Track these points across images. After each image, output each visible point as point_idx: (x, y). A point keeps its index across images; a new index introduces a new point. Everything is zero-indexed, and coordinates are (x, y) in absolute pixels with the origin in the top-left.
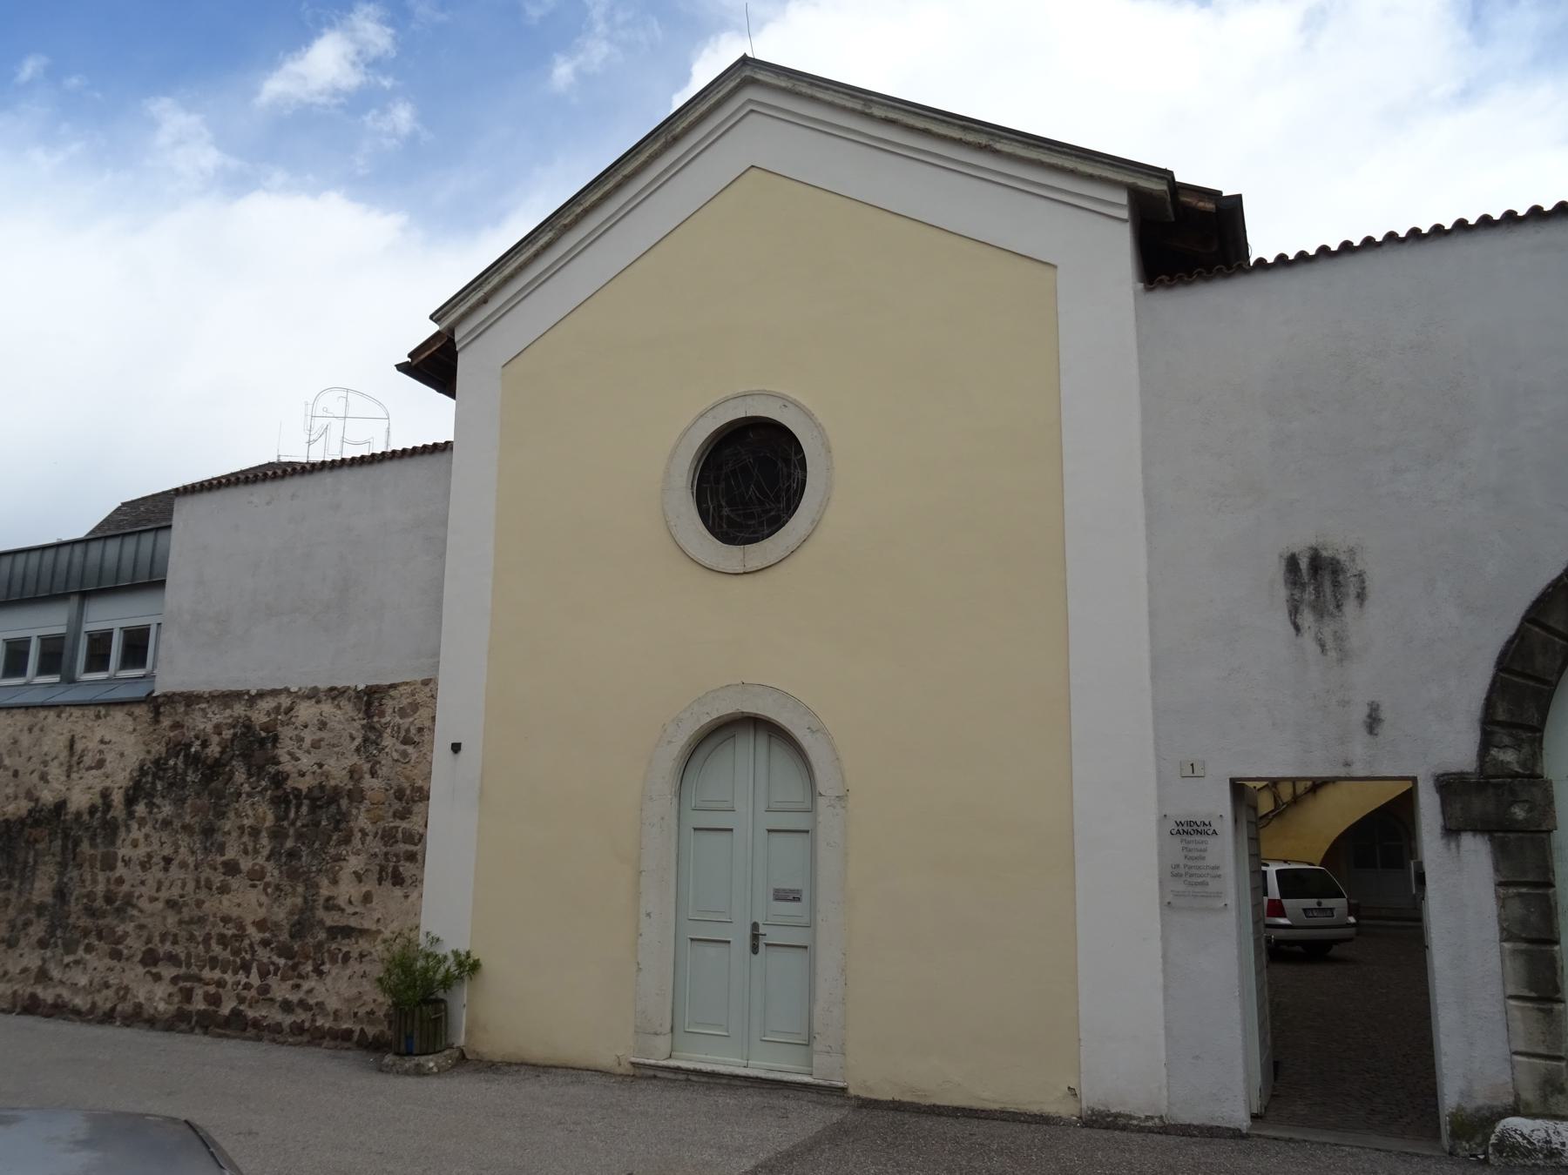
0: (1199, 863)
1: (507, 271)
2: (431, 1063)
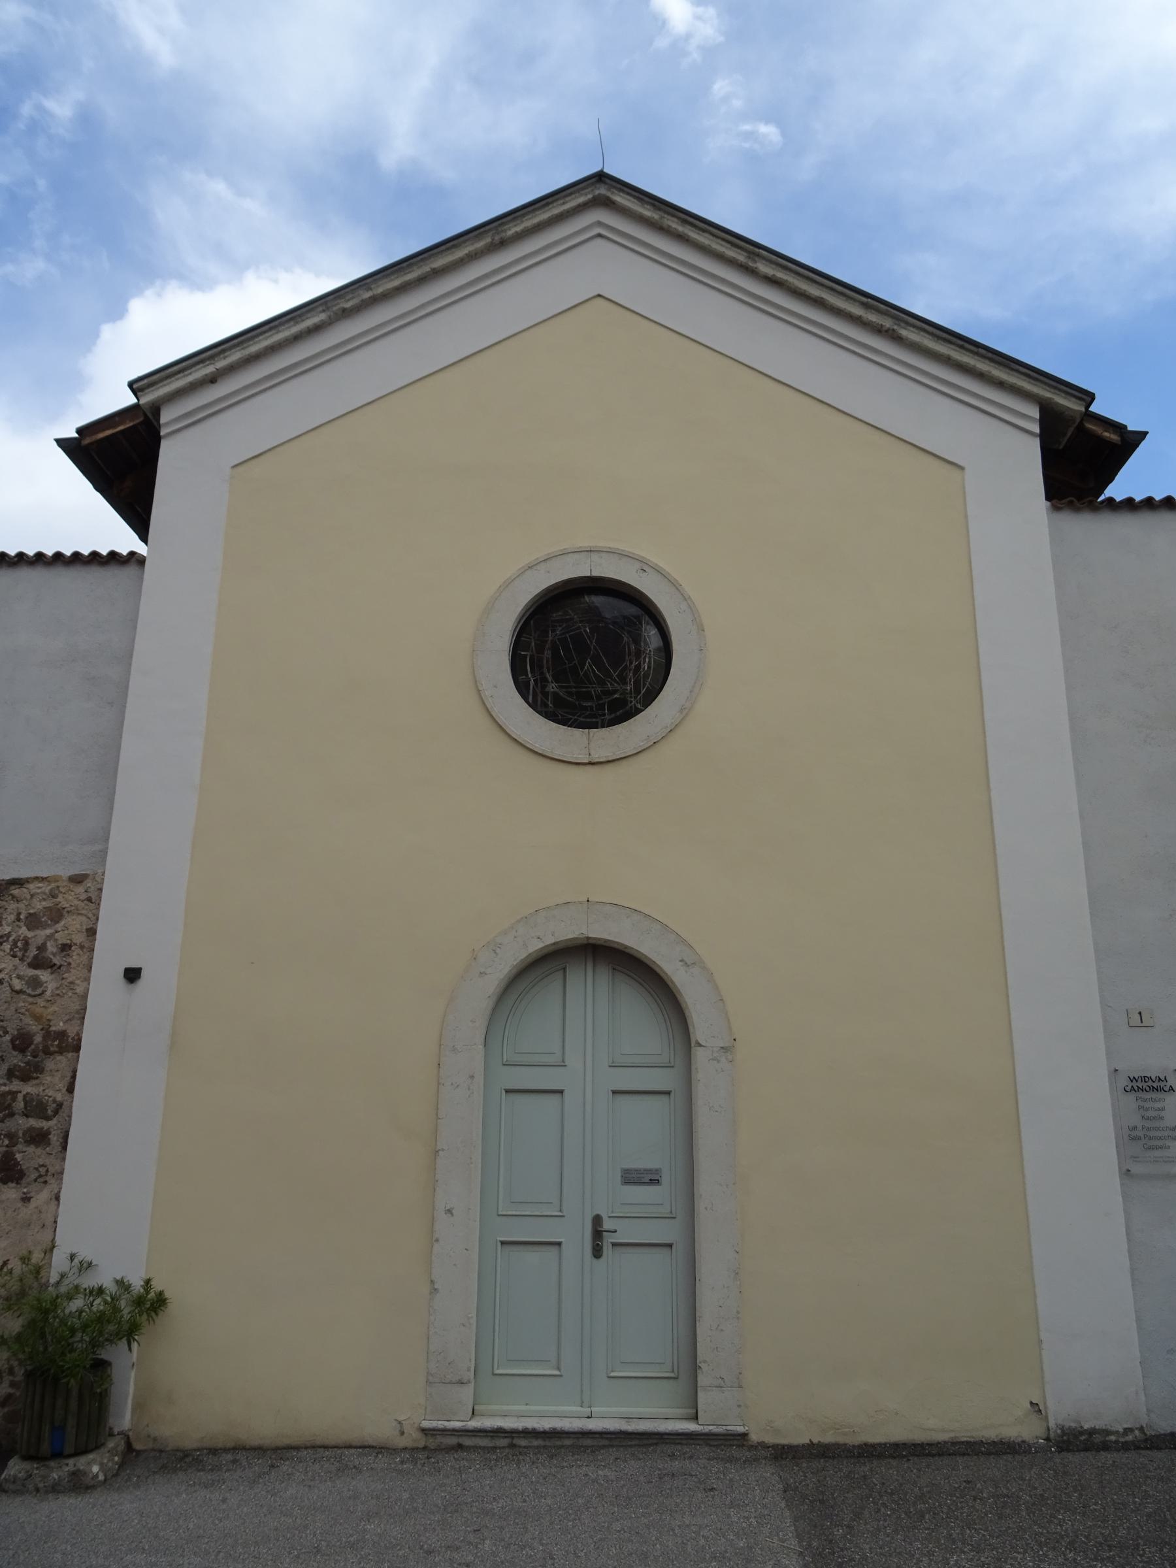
0: (1157, 1124)
1: (254, 348)
2: (94, 1466)
